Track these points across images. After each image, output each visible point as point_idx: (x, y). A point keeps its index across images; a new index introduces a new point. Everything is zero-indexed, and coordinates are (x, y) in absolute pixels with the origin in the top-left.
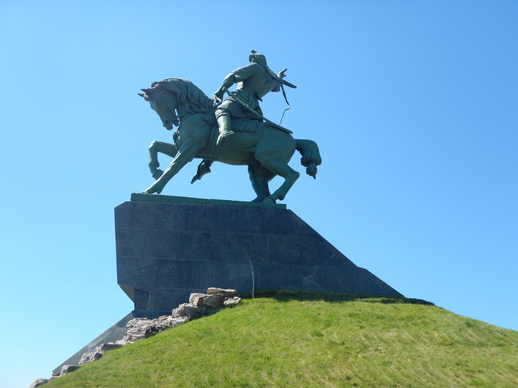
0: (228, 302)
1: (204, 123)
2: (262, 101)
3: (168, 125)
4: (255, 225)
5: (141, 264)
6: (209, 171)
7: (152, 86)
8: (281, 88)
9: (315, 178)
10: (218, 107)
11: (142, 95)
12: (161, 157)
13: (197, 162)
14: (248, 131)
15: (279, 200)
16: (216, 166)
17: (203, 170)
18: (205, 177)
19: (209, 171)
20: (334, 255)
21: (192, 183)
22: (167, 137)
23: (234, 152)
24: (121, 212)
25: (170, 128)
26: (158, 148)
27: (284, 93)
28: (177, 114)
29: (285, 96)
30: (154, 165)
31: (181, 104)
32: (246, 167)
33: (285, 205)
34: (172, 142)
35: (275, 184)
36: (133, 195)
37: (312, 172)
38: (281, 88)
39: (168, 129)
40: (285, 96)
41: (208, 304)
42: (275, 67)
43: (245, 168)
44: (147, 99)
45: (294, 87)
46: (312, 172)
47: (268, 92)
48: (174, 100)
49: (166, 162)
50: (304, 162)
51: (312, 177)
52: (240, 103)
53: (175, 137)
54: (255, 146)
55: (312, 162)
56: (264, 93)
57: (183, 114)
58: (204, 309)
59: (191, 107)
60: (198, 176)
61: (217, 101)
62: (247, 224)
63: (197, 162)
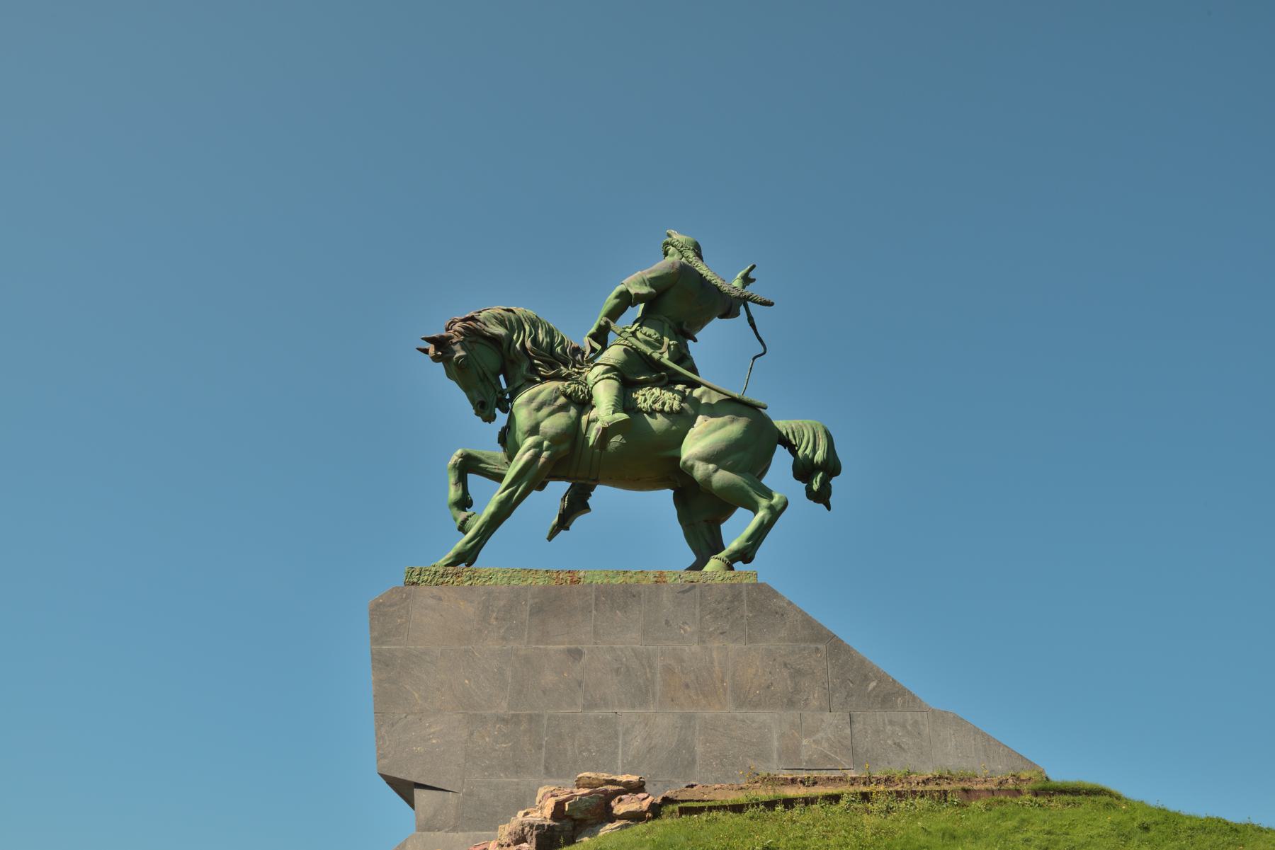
0: (619, 808)
2: (695, 340)
4: (685, 623)
5: (430, 726)
6: (586, 508)
8: (742, 308)
9: (829, 508)
10: (597, 361)
11: (426, 351)
13: (558, 490)
15: (740, 563)
16: (602, 495)
17: (576, 505)
18: (580, 522)
19: (586, 508)
20: (873, 684)
21: (550, 539)
25: (490, 418)
27: (750, 319)
28: (504, 386)
29: (753, 325)
31: (512, 362)
32: (669, 493)
37: (822, 497)
38: (742, 308)
39: (485, 420)
40: (753, 325)
41: (578, 816)
43: (667, 494)
44: (436, 359)
45: (769, 304)
46: (822, 497)
47: (709, 319)
51: (822, 506)
52: (645, 354)
55: (818, 475)
56: (701, 324)
57: (517, 385)
58: (569, 826)
60: (564, 521)
61: (593, 350)
62: (667, 622)
63: (558, 490)
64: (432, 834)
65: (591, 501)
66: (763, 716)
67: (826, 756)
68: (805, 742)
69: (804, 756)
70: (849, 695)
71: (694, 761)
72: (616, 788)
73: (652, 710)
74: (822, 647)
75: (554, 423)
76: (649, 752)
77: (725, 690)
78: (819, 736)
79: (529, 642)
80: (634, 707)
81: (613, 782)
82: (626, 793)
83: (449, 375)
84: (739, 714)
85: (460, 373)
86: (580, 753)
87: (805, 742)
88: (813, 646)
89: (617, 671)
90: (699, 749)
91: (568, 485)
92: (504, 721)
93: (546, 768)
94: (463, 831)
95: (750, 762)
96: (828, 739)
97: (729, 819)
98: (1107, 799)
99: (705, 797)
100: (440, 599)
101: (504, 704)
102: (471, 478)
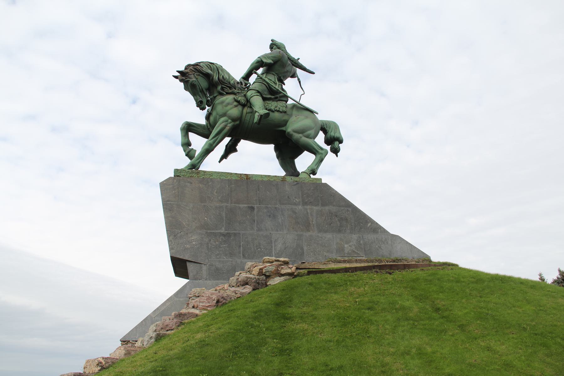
1: (235, 103)
3: (200, 105)
6: (236, 150)
7: (186, 69)
9: (337, 156)
11: (176, 77)
12: (193, 137)
14: (278, 111)
17: (231, 149)
18: (232, 156)
19: (236, 150)
20: (369, 224)
21: (220, 162)
22: (199, 117)
23: (263, 132)
24: (164, 186)
26: (189, 128)
29: (300, 82)
30: (187, 144)
32: (272, 146)
33: (321, 179)
34: (203, 122)
35: (304, 162)
36: (176, 171)
37: (336, 151)
39: (201, 109)
40: (300, 82)
42: (293, 52)
46: (336, 151)
48: (203, 82)
49: (198, 143)
50: (329, 141)
53: (208, 118)
54: (286, 125)
55: (334, 142)
57: (215, 95)
59: (222, 89)
62: (288, 197)
64: (197, 281)
65: (237, 147)
66: (329, 236)
67: (354, 251)
68: (346, 246)
69: (346, 251)
70: (361, 228)
71: (303, 252)
72: (280, 263)
73: (285, 232)
74: (350, 209)
75: (235, 112)
76: (285, 249)
77: (314, 225)
78: (351, 244)
79: (231, 203)
80: (277, 231)
81: (278, 261)
82: (282, 265)
83: (186, 89)
84: (320, 235)
85: (191, 87)
86: (257, 249)
87: (346, 246)
88: (346, 209)
89: (270, 216)
90: (305, 248)
91: (230, 138)
92: (224, 235)
93: (243, 255)
94: (210, 280)
95: (325, 254)
96: (354, 245)
97: (376, 278)
98: (452, 267)
99: (311, 267)
100: (191, 183)
101: (223, 229)
102: (191, 135)
